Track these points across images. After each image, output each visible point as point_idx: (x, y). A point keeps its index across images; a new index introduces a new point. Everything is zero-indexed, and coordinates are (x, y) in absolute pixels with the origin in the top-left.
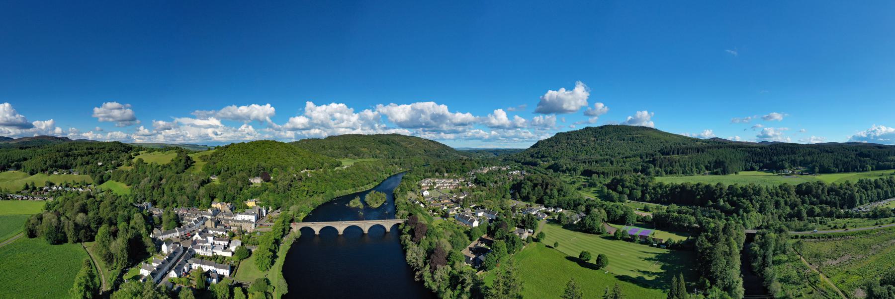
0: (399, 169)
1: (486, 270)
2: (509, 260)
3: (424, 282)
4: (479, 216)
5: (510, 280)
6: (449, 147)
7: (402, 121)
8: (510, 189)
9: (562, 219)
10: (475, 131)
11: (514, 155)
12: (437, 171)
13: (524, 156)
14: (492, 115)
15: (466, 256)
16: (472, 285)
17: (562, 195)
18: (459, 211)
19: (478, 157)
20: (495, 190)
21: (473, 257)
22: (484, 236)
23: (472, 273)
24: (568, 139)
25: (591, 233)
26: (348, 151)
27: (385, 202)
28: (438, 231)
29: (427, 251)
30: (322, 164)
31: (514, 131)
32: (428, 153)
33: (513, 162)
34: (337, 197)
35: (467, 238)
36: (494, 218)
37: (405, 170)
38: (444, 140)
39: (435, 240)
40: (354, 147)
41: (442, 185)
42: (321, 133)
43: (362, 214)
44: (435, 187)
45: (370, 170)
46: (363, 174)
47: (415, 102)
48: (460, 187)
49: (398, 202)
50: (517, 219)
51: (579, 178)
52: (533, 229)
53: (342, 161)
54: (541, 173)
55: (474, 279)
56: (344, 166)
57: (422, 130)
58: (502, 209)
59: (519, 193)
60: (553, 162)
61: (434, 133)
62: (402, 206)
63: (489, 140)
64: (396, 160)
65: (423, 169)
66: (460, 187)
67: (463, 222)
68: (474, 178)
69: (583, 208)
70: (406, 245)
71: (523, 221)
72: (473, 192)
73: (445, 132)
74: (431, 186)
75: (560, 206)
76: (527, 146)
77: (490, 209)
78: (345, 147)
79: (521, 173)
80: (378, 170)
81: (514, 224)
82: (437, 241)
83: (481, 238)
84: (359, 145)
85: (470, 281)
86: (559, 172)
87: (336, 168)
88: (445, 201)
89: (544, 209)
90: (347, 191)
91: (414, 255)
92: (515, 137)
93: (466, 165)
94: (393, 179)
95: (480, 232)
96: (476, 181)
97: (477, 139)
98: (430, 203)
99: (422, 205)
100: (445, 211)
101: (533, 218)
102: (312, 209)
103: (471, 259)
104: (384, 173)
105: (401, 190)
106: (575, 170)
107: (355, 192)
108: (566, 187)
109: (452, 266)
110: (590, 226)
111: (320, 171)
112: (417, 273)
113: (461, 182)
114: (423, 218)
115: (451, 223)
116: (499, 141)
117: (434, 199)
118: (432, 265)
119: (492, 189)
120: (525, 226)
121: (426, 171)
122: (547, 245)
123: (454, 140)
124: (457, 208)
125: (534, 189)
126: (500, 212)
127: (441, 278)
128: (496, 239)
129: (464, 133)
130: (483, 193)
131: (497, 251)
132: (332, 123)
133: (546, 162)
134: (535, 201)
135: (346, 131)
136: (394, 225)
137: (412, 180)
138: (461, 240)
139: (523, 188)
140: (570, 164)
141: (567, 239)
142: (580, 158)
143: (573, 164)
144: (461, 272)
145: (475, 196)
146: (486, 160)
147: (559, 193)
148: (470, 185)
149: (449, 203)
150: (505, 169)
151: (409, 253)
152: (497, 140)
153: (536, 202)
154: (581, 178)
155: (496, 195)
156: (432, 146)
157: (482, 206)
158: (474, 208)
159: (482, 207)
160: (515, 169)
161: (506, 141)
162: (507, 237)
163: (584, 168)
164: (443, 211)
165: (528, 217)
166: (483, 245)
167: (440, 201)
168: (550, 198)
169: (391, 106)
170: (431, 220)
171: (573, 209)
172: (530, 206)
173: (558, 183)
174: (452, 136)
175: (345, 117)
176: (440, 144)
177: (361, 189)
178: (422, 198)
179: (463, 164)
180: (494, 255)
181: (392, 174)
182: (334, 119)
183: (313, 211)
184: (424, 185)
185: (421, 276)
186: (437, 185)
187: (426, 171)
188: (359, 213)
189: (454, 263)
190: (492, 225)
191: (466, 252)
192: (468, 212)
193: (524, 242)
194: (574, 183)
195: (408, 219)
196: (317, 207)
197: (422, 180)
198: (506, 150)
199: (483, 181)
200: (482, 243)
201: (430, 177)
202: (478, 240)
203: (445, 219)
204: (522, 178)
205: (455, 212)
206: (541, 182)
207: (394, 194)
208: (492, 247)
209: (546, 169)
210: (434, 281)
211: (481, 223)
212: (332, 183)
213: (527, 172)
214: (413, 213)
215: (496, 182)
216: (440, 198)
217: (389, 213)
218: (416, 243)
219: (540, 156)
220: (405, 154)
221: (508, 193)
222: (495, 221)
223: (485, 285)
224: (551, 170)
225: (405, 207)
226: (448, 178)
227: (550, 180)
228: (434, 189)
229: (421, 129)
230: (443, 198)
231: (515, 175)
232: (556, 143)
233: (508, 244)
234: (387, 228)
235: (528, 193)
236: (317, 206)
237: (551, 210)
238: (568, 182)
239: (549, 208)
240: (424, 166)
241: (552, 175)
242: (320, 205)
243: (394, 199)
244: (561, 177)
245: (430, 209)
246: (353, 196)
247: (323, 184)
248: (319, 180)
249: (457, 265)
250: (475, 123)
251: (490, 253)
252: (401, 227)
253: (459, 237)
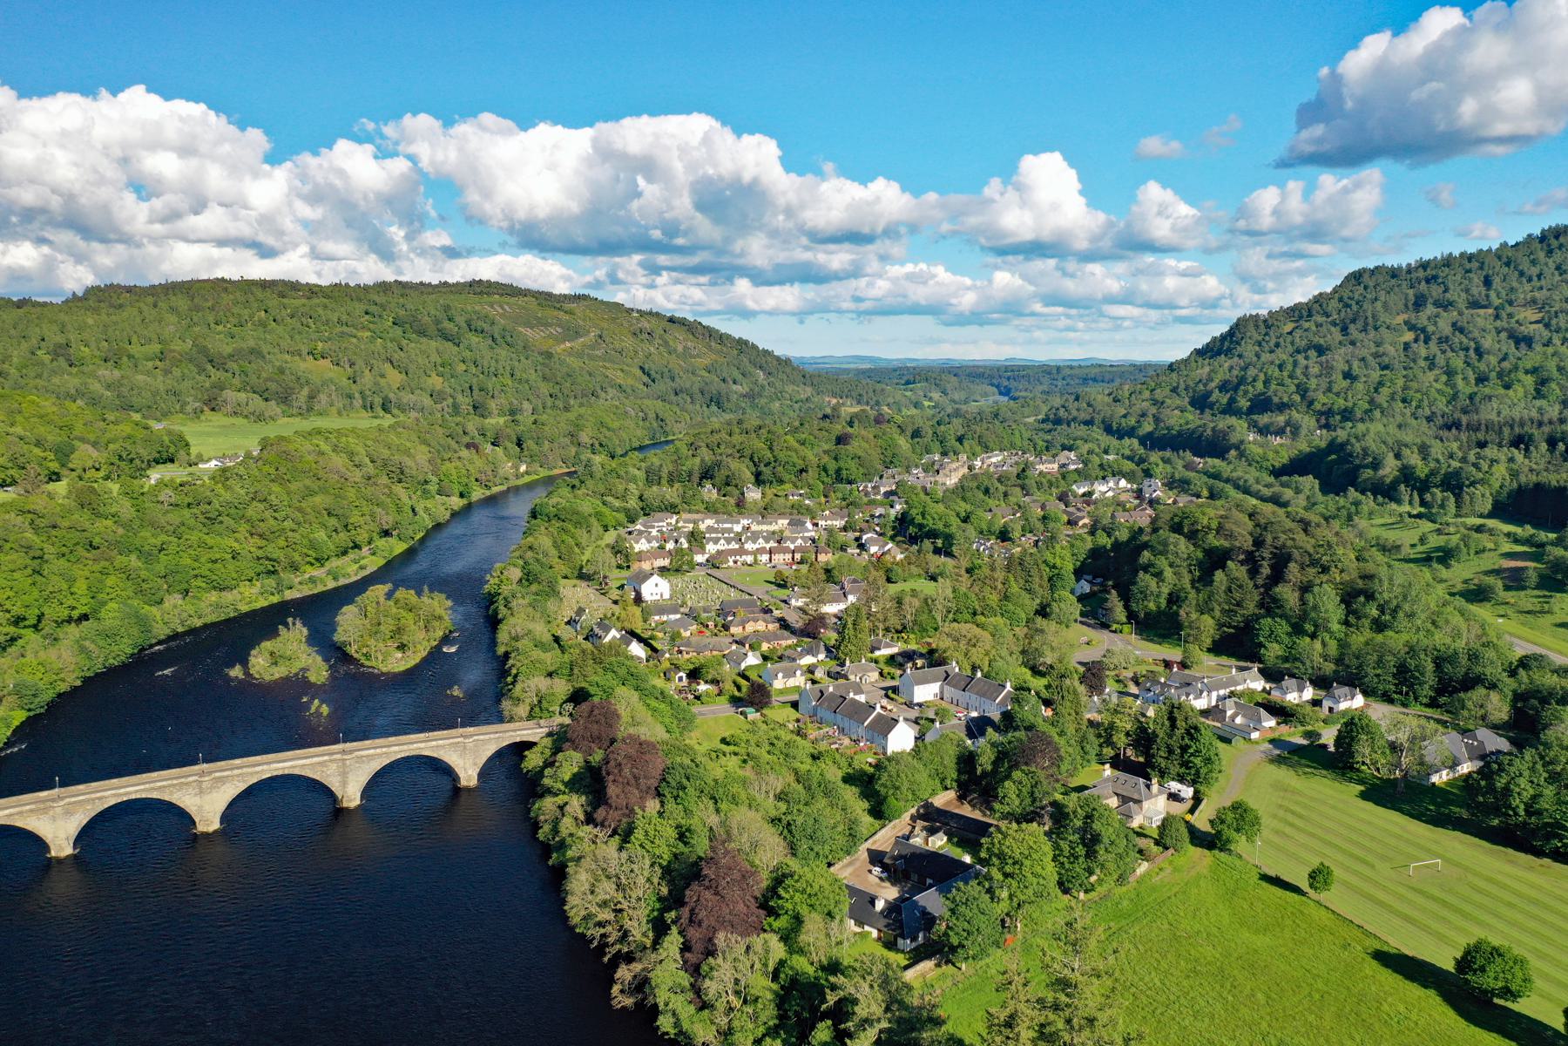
0: (511, 469)
1: (948, 962)
2: (1069, 924)
3: (654, 1011)
4: (916, 700)
5: (1069, 1021)
6: (766, 353)
7: (542, 213)
8: (1079, 573)
9: (1363, 751)
10: (909, 268)
11: (1098, 395)
12: (707, 475)
13: (1155, 402)
14: (1005, 183)
15: (853, 891)
16: (885, 1025)
17: (1366, 622)
18: (819, 674)
19: (916, 405)
20: (1000, 575)
21: (888, 893)
22: (944, 799)
23: (884, 974)
24: (1419, 303)
25: (1538, 853)
26: (216, 375)
27: (446, 640)
28: (719, 773)
29: (667, 871)
30: (64, 454)
31: (1120, 267)
32: (662, 386)
33: (1097, 433)
34: (175, 636)
35: (859, 807)
36: (995, 715)
37: (543, 473)
38: (747, 314)
39: (704, 816)
40: (252, 351)
41: (736, 546)
42: (49, 266)
43: (325, 710)
44: (700, 558)
45: (357, 475)
46: (318, 499)
47: (615, 116)
48: (822, 558)
49: (516, 639)
50: (1112, 726)
51: (1479, 529)
52: (1194, 783)
53: (189, 430)
54: (1246, 491)
55: (893, 1001)
56: (201, 459)
57: (642, 264)
58: (1036, 671)
59: (1126, 598)
60: (1321, 438)
61: (703, 279)
62: (537, 654)
63: (976, 318)
64: (496, 421)
65: (635, 468)
66: (822, 558)
67: (842, 731)
68: (893, 512)
69: (1499, 707)
70: (562, 846)
71: (1143, 738)
72: (889, 580)
73: (760, 278)
74: (679, 551)
75: (1353, 680)
76: (1176, 345)
77: (974, 668)
78: (204, 351)
79: (1139, 494)
80: (400, 475)
81: (1093, 749)
82: (713, 820)
83: (928, 806)
84: (284, 344)
85: (877, 1010)
86: (1352, 493)
87: (155, 475)
88: (750, 627)
89: (1258, 684)
90: (228, 597)
91: (607, 889)
92: (1126, 299)
93: (854, 447)
94: (479, 517)
95: (922, 776)
96: (906, 530)
97: (916, 310)
98: (675, 637)
99: (636, 649)
100: (753, 676)
101: (1196, 728)
102: (19, 717)
103: (880, 905)
104: (433, 488)
105: (528, 578)
106: (1454, 484)
107: (275, 599)
108: (1394, 579)
109: (787, 938)
110: (1539, 813)
111: (51, 496)
112: (624, 973)
113: (829, 530)
114: (642, 712)
115: (781, 733)
116: (1027, 321)
117: (693, 615)
118: (694, 934)
119: (986, 571)
120: (1149, 763)
121: (652, 477)
122: (1272, 873)
123: (801, 315)
124: (808, 660)
125: (1204, 577)
126: (1021, 688)
127: (737, 993)
128: (1005, 816)
129: (853, 283)
130: (940, 591)
131: (1006, 875)
132: (135, 214)
133: (1280, 432)
134: (1208, 642)
135: (214, 263)
136: (499, 754)
137: (581, 521)
138: (831, 817)
139: (1146, 568)
140: (1424, 451)
141: (1383, 858)
142: (1493, 417)
143: (1446, 452)
144: (833, 967)
145: (899, 602)
146: (956, 422)
147: (1349, 612)
148: (874, 549)
149: (768, 637)
150: (1056, 466)
151: (579, 881)
152: (1020, 314)
153: (1217, 648)
154: (1491, 532)
155: (1006, 597)
156: (680, 348)
157: (932, 652)
158: (891, 660)
159: (934, 659)
160: (1107, 471)
161: (1064, 322)
162: (1060, 815)
163: (1514, 474)
164: (743, 675)
165: (1172, 720)
166: (939, 842)
167: (726, 627)
168: (1297, 630)
169: (483, 128)
170: (685, 721)
171: (1433, 704)
172: (1183, 665)
173: (1347, 556)
174: (787, 296)
175: (215, 178)
176: (722, 338)
177: (312, 580)
178: (637, 611)
179: (841, 440)
180: (990, 891)
181: (478, 494)
182: (143, 188)
183: (20, 733)
184: (642, 546)
185: (641, 985)
186: (711, 548)
187: (652, 477)
188: (308, 705)
189: (798, 920)
190: (985, 750)
191: (855, 871)
192: (865, 682)
193: (1142, 843)
194: (1445, 556)
195: (567, 721)
196: (51, 705)
197: (632, 521)
198: (1058, 369)
199: (940, 526)
200: (932, 831)
201: (672, 509)
202: (913, 818)
203: (753, 715)
204: (1143, 518)
205: (799, 680)
206: (1248, 544)
207: (491, 599)
208: (983, 855)
209: (1277, 473)
210: (704, 1006)
211: (929, 738)
212: (134, 561)
213: (1171, 484)
214: (592, 690)
215: (1004, 536)
216: (722, 612)
217: (472, 695)
218: (615, 833)
219: (1244, 403)
220: (544, 388)
221: (1066, 594)
222: (996, 728)
223: (948, 1028)
224: (1309, 483)
225: (551, 658)
226: (766, 512)
227: (1300, 537)
228: (692, 566)
229: (637, 258)
230: (741, 613)
231: (1103, 501)
232: (1344, 330)
233: (1064, 845)
234: (462, 775)
235: (1175, 599)
236: (49, 695)
237: (1297, 695)
238: (1407, 551)
239: (1288, 682)
240: (641, 448)
241: (1311, 505)
242: (63, 687)
243: (494, 622)
244: (1362, 523)
245: (677, 668)
246: (266, 622)
247: (79, 572)
248: (49, 549)
249: (813, 932)
250: (914, 228)
251: (974, 883)
252: (533, 760)
253: (821, 803)
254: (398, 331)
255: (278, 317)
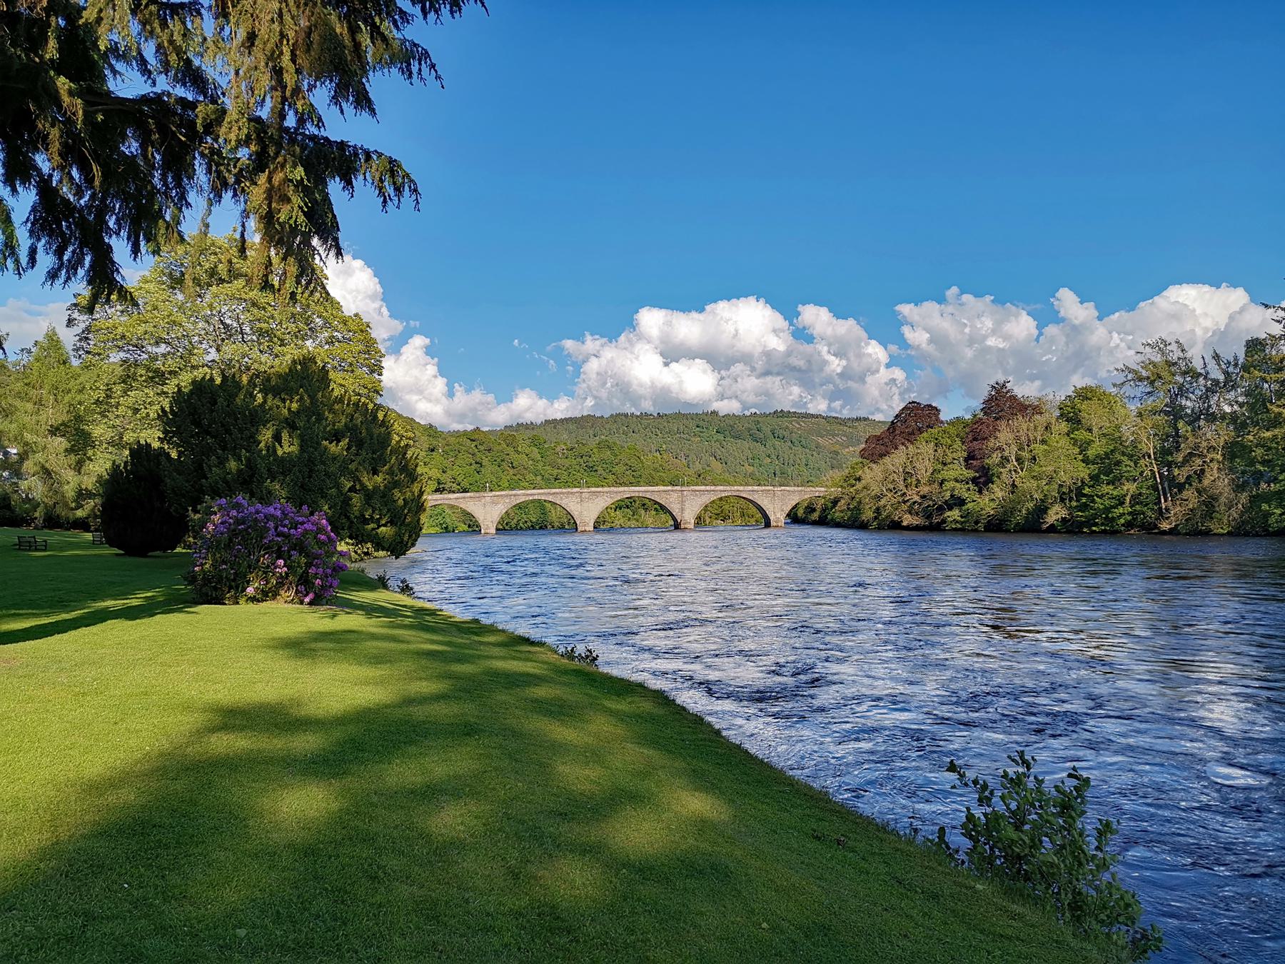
254: (721, 437)
255: (636, 430)
